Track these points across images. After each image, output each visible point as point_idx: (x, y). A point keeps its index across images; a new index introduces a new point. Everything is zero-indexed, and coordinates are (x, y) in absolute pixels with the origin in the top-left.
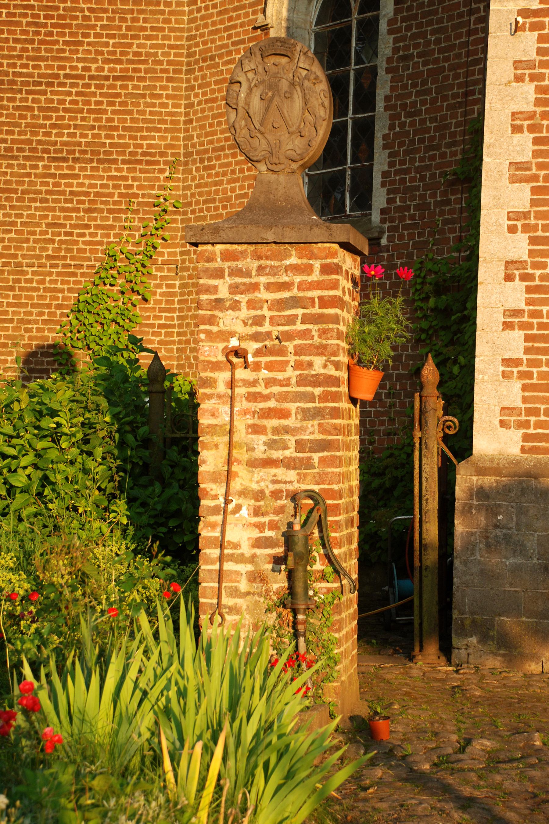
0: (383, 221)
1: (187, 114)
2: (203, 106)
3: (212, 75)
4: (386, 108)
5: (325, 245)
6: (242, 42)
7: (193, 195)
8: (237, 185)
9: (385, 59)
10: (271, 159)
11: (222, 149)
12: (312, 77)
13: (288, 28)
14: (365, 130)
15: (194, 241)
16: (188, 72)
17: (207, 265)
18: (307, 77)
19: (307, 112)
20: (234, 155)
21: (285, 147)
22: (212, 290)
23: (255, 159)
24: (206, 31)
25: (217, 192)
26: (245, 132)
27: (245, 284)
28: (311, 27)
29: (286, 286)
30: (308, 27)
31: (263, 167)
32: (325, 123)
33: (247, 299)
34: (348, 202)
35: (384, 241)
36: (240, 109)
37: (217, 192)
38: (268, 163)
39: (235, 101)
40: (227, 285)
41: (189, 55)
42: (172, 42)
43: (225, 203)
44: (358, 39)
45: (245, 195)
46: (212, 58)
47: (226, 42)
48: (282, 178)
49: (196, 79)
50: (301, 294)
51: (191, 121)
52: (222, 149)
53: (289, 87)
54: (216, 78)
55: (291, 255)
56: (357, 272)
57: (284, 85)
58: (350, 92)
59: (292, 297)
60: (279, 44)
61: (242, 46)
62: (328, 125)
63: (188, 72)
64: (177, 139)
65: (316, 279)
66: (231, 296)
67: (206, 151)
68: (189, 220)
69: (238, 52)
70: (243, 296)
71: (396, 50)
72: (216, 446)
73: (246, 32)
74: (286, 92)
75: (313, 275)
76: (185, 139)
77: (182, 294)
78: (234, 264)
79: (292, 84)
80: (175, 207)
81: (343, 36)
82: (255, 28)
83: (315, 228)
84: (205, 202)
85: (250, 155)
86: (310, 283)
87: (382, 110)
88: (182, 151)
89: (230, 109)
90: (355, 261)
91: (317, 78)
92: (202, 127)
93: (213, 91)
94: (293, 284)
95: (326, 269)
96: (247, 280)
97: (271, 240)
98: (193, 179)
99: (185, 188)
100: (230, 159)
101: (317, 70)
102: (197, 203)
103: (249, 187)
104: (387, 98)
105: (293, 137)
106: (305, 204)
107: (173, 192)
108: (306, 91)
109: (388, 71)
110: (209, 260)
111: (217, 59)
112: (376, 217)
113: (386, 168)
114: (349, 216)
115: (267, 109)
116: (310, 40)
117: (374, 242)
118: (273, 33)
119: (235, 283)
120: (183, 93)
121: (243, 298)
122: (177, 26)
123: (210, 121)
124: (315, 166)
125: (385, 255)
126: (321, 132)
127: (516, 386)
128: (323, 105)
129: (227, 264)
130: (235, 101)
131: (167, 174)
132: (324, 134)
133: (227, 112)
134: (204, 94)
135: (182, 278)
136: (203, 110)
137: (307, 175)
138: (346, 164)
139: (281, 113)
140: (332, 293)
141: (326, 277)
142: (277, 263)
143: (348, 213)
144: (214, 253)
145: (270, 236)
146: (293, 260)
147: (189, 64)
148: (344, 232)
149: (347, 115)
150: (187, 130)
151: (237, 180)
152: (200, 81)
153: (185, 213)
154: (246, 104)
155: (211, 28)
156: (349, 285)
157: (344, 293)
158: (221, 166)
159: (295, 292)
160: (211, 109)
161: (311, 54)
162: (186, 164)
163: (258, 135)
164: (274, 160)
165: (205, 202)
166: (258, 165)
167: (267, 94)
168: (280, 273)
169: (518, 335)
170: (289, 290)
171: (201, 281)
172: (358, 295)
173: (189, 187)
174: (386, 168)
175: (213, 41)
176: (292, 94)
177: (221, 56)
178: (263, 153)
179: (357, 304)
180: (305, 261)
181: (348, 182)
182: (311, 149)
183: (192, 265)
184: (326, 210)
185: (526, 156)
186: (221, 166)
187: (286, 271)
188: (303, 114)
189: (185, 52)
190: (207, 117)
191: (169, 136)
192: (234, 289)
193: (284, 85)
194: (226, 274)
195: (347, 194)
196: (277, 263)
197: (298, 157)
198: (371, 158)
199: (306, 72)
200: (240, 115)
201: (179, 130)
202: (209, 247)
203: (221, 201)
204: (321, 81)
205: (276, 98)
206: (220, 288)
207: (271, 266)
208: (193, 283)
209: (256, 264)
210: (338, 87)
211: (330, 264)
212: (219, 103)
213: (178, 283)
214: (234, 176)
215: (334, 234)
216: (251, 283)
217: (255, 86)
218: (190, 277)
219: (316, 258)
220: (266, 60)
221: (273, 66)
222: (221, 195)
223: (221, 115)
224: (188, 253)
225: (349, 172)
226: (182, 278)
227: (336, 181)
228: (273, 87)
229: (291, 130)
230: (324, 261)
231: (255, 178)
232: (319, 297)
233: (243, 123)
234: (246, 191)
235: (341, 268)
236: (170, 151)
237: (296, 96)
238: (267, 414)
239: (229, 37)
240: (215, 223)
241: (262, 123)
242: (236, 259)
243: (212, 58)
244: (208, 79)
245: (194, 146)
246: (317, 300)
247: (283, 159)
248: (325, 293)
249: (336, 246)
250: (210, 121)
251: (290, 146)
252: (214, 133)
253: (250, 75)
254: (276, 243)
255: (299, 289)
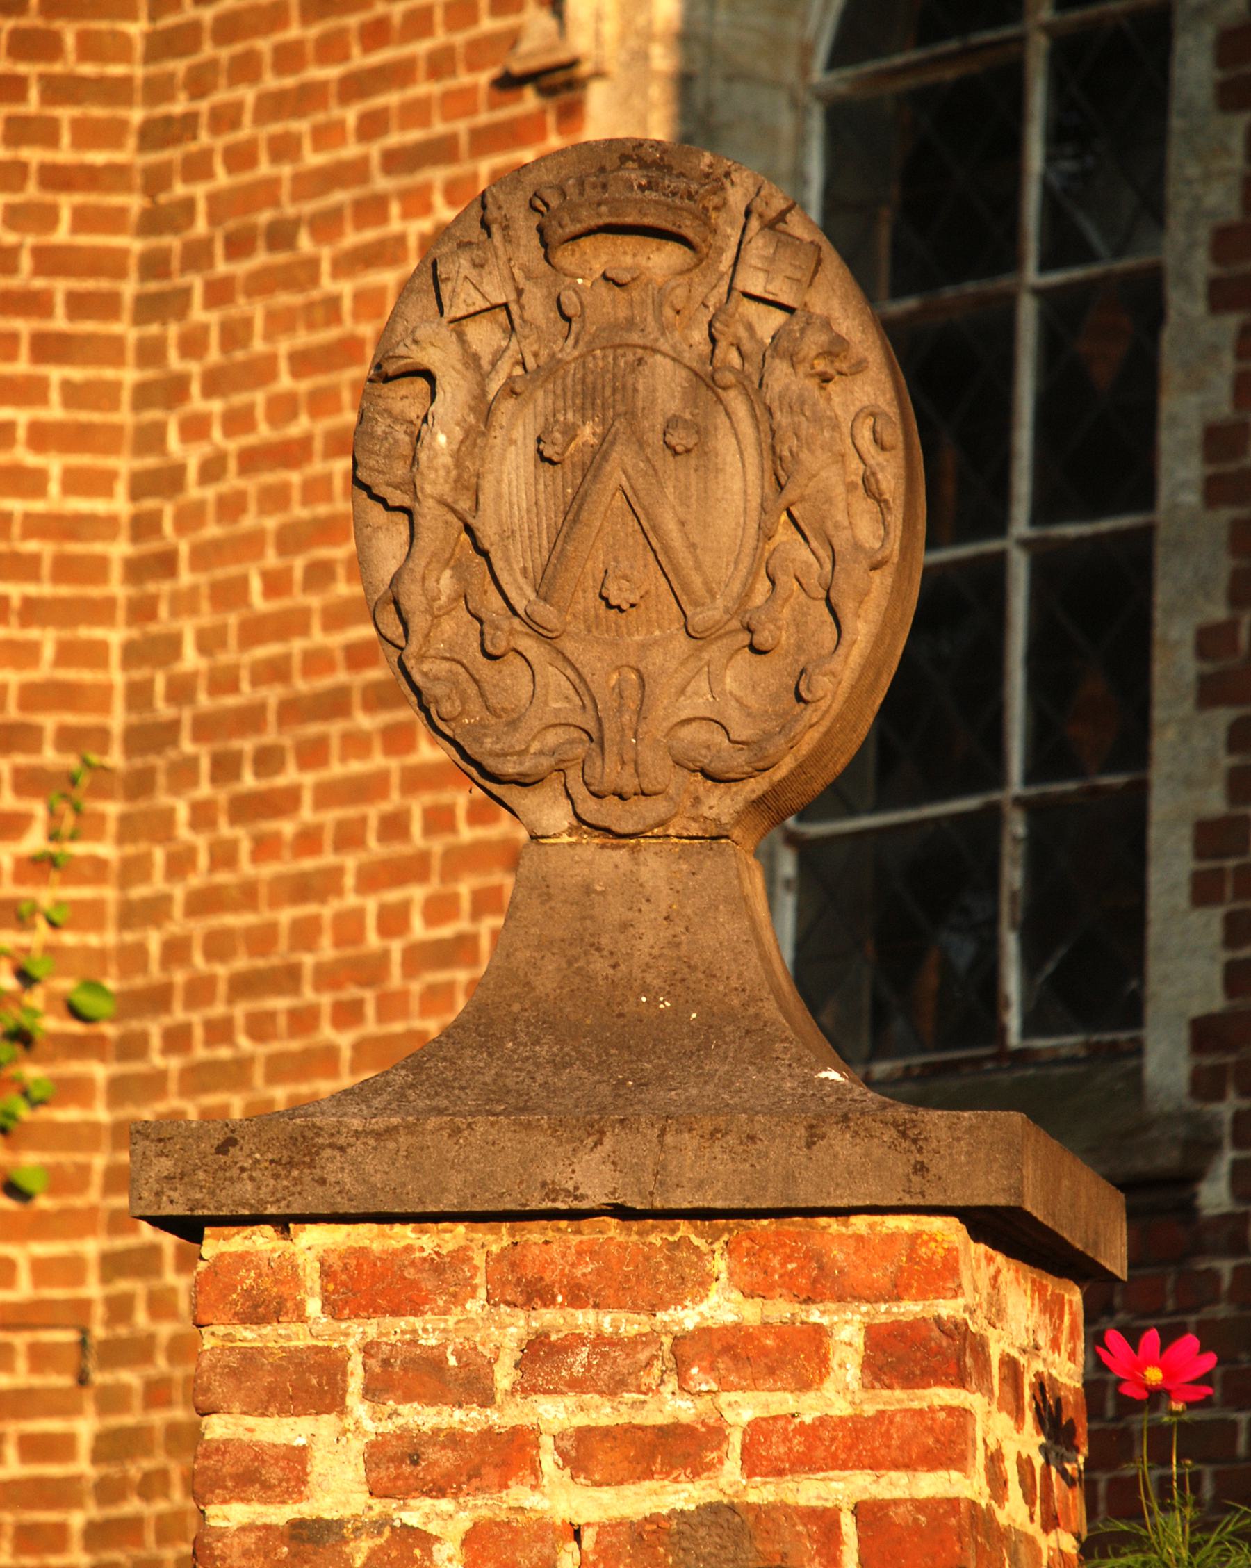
0: (1206, 1085)
1: (144, 526)
2: (232, 481)
3: (279, 322)
4: (1216, 491)
5: (893, 1223)
6: (442, 151)
7: (175, 951)
8: (417, 893)
9: (1203, 233)
10: (595, 771)
11: (334, 704)
12: (814, 342)
13: (684, 82)
14: (1100, 609)
15: (179, 1210)
16: (149, 308)
17: (248, 1335)
18: (783, 347)
19: (784, 526)
20: (397, 740)
21: (669, 708)
22: (273, 1474)
23: (510, 767)
24: (248, 95)
25: (305, 934)
26: (455, 628)
27: (454, 1439)
28: (805, 70)
29: (680, 1448)
30: (790, 73)
31: (554, 816)
32: (881, 582)
33: (464, 1521)
34: (1012, 983)
35: (1215, 1195)
36: (429, 512)
37: (305, 934)
38: (579, 791)
39: (400, 470)
40: (358, 1445)
41: (152, 223)
42: (65, 155)
43: (351, 992)
44: (1057, 136)
45: (459, 950)
46: (281, 236)
47: (351, 150)
48: (654, 867)
49: (192, 345)
50: (762, 1493)
51: (166, 564)
52: (334, 704)
53: (691, 398)
54: (303, 339)
55: (705, 1281)
56: (1067, 1372)
57: (664, 387)
58: (1015, 397)
59: (712, 1509)
60: (636, 176)
61: (438, 175)
62: (896, 593)
63: (149, 308)
64: (94, 654)
65: (841, 1409)
66: (379, 1506)
67: (250, 719)
68: (154, 1084)
69: (417, 203)
70: (445, 1505)
72: (771, 195)
73: (459, 102)
74: (672, 423)
75: (829, 1387)
76: (133, 654)
77: (108, 1491)
78: (392, 1329)
79: (706, 381)
80: (75, 1013)
82: (508, 83)
83: (833, 1131)
84: (243, 986)
85: (485, 748)
86: (811, 1432)
87: (1192, 498)
88: (117, 719)
89: (376, 513)
90: (1053, 1308)
91: (836, 348)
92: (229, 594)
93: (283, 408)
94: (716, 1434)
95: (900, 1356)
96: (466, 1418)
97: (596, 1198)
98: (179, 864)
99: (132, 915)
100: (378, 761)
101: (839, 307)
102: (200, 992)
103: (484, 902)
105: (714, 652)
106: (780, 1006)
107: (68, 939)
108: (782, 418)
109: (1221, 297)
110: (261, 1310)
111: (305, 242)
112: (1166, 1063)
113: (1215, 803)
114: (1022, 1057)
115: (573, 511)
116: (801, 140)
117: (1157, 1200)
118: (603, 117)
119: (403, 1434)
120: (125, 416)
122: (88, 69)
123: (271, 559)
124: (838, 797)
125: (1225, 1267)
126: (862, 629)
128: (870, 487)
129: (356, 1333)
130: (400, 470)
131: (35, 841)
132: (878, 641)
133: (358, 519)
134: (238, 421)
135: (111, 1400)
136: (231, 507)
137: (792, 839)
138: (998, 779)
139: (649, 533)
140: (932, 1484)
141: (897, 1399)
142: (630, 1324)
143: (1014, 1039)
144: (288, 1273)
145: (593, 1179)
146: (721, 1306)
147: (154, 265)
148: (987, 1151)
149: (998, 525)
150: (142, 611)
151: (415, 869)
152: (214, 355)
153: (132, 1047)
154: (459, 484)
155: (271, 82)
156: (1023, 1441)
157: (997, 1483)
158: (327, 795)
159: (729, 1479)
160: (275, 498)
161: (803, 228)
162: (139, 784)
163: (528, 645)
164: (612, 773)
165: (243, 986)
166: (524, 800)
167: (570, 432)
168: (650, 1378)
170: (698, 1469)
171: (217, 1428)
172: (1076, 1498)
173: (155, 911)
174: (1215, 803)
175: (284, 148)
176: (702, 432)
177: (326, 225)
178: (553, 738)
179: (1069, 1544)
180: (781, 1310)
181: (1013, 876)
182: (810, 715)
183: (165, 1330)
184: (898, 1026)
186: (327, 795)
187: (681, 1368)
188: (766, 534)
189: (135, 203)
190: (251, 544)
191: (47, 638)
193: (664, 387)
194: (355, 1383)
195: (1011, 944)
196: (630, 1324)
197: (740, 760)
198: (1133, 748)
199: (779, 317)
200: (426, 540)
201: (101, 611)
202: (263, 1240)
203: (327, 977)
204: (859, 367)
205: (623, 457)
206: (318, 1465)
207: (600, 1340)
208: (173, 1431)
209: (513, 1329)
210: (947, 389)
211: (917, 1324)
212: (317, 467)
213: (85, 1428)
214: (398, 849)
215: (939, 1166)
216: (488, 1434)
217: (510, 390)
218: (157, 1394)
219: (844, 1296)
220: (566, 258)
221: (603, 290)
222: (327, 950)
223: (326, 530)
224: (145, 1262)
225: (1017, 826)
226: (111, 1400)
227: (949, 872)
228: (605, 396)
229: (699, 618)
230: (885, 1312)
231: (511, 857)
232: (860, 1510)
233: (446, 583)
234: (462, 925)
235: (979, 1347)
236: (49, 722)
237: (724, 444)
239: (372, 126)
240: (296, 1108)
241: (545, 586)
242: (405, 1300)
243: (281, 236)
244: (259, 345)
245: (181, 691)
246: (848, 1525)
247: (659, 772)
248: (896, 1486)
249: (949, 1230)
250: (271, 559)
251: (698, 702)
252: (293, 624)
253: (484, 336)
254: (622, 1213)
255: (751, 1464)
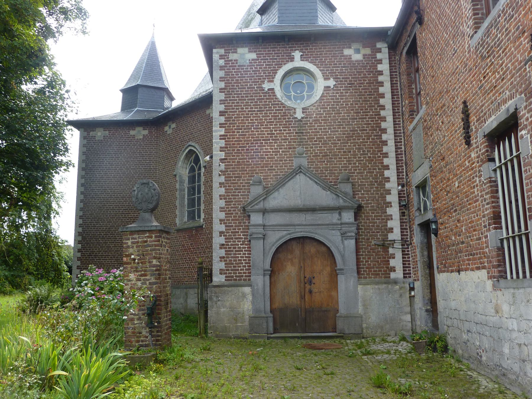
35: (204, 227)
71: (205, 180)
81: (194, 176)
104: (204, 191)
112: (202, 220)
121: (135, 245)
127: (223, 263)
169: (223, 250)
185: (223, 205)
192: (133, 243)
238: (141, 275)
